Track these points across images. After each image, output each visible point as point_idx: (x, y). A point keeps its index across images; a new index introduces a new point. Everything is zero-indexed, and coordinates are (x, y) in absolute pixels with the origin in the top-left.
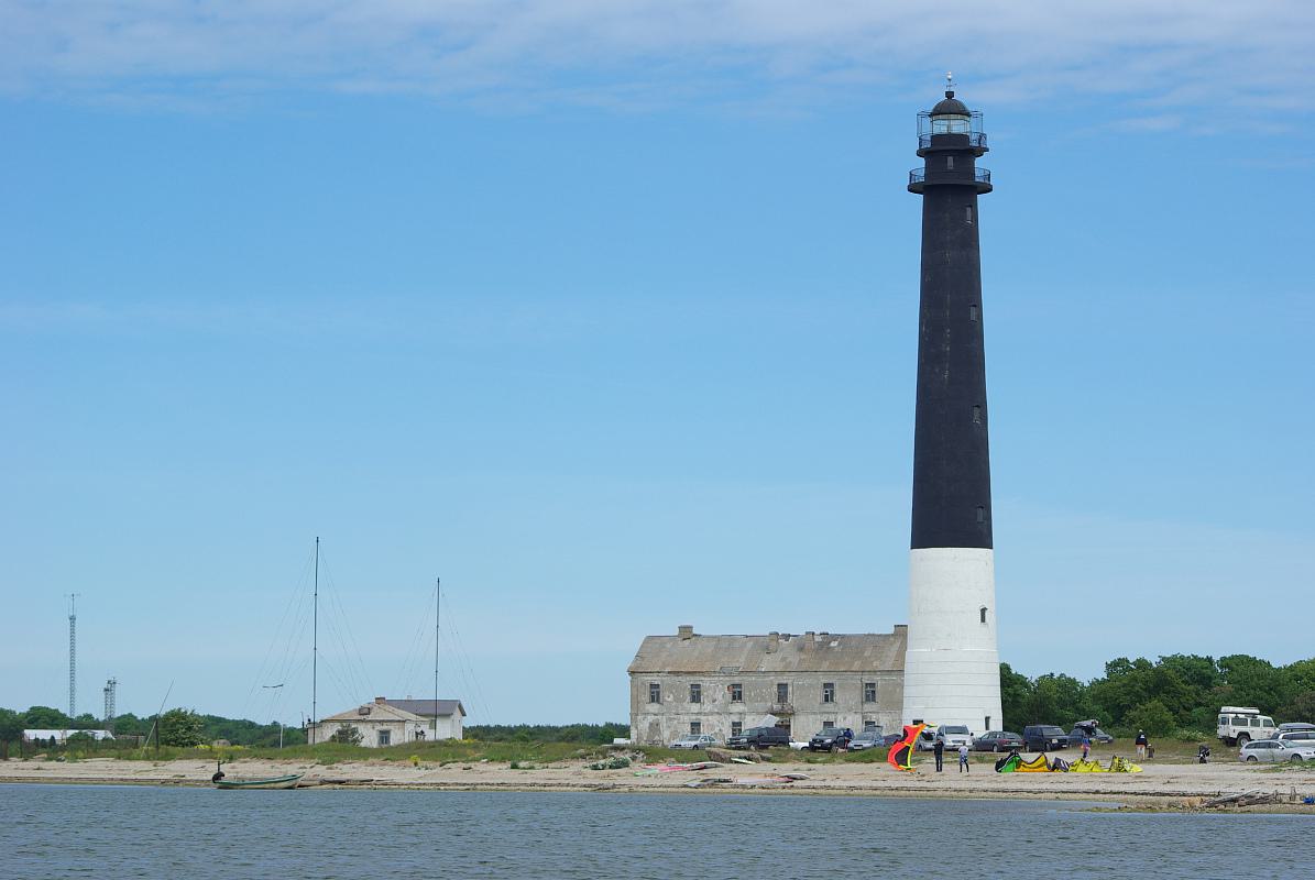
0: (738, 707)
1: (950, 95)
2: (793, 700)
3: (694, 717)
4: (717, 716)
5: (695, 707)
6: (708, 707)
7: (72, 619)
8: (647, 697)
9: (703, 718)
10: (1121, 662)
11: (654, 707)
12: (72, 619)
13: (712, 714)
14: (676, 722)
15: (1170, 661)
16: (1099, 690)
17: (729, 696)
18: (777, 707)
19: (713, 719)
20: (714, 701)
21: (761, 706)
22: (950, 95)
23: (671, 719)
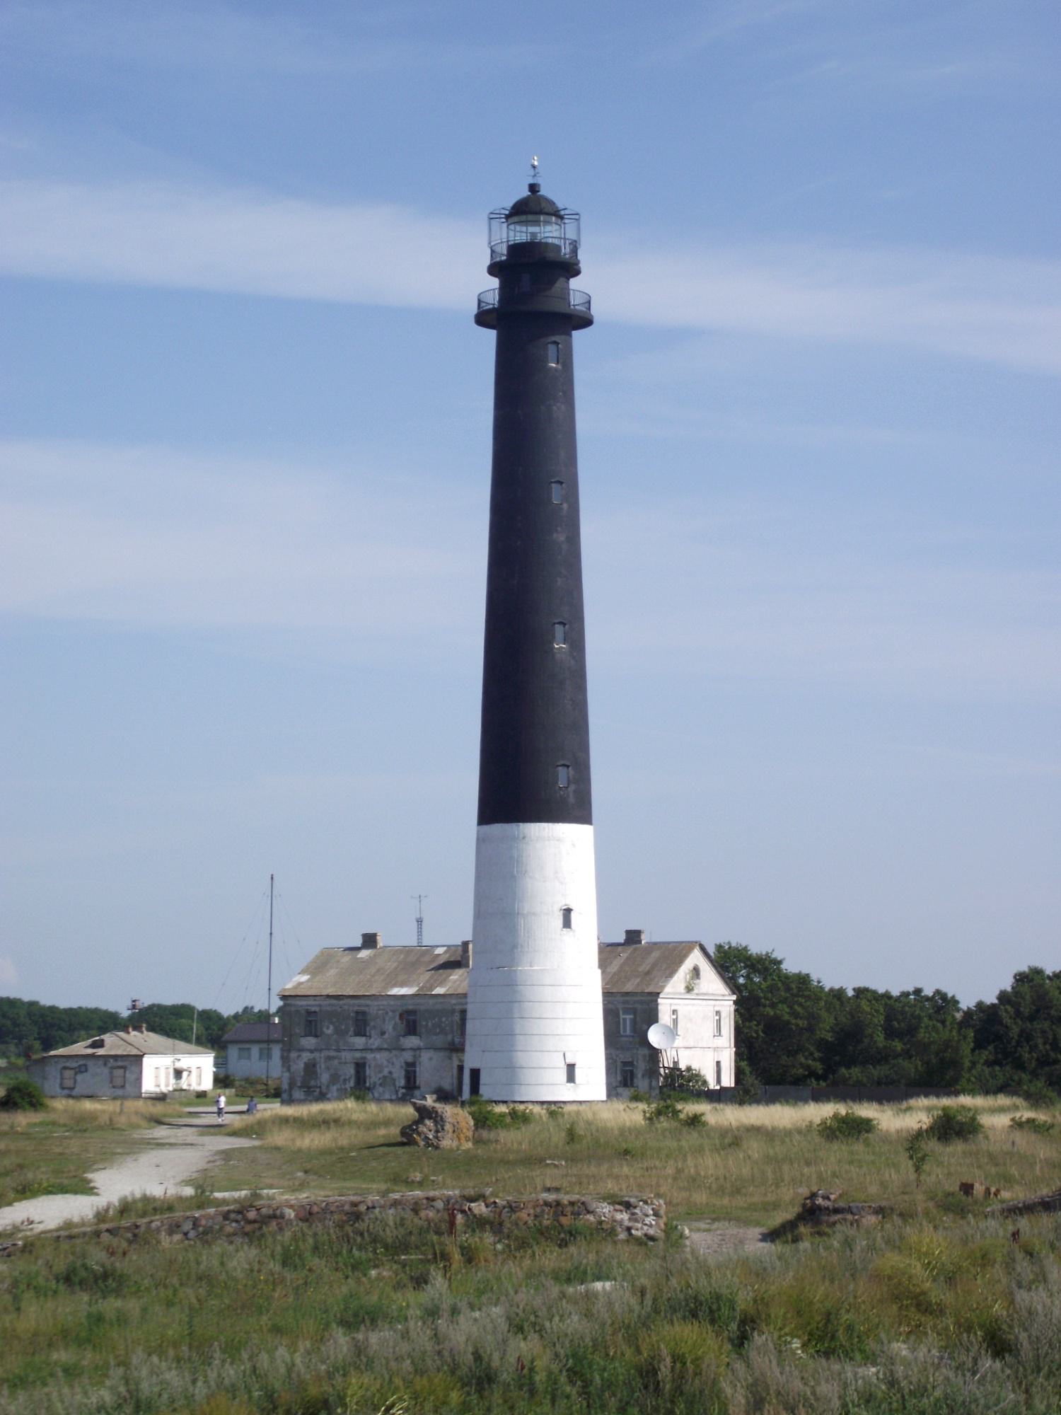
0: (413, 1041)
1: (533, 188)
3: (358, 1055)
4: (385, 1054)
5: (359, 1041)
7: (420, 921)
9: (369, 1056)
11: (309, 1042)
12: (420, 921)
13: (380, 1049)
14: (336, 1061)
15: (861, 992)
16: (986, 1022)
17: (402, 1027)
19: (381, 1057)
20: (383, 1033)
22: (533, 188)
23: (329, 1058)
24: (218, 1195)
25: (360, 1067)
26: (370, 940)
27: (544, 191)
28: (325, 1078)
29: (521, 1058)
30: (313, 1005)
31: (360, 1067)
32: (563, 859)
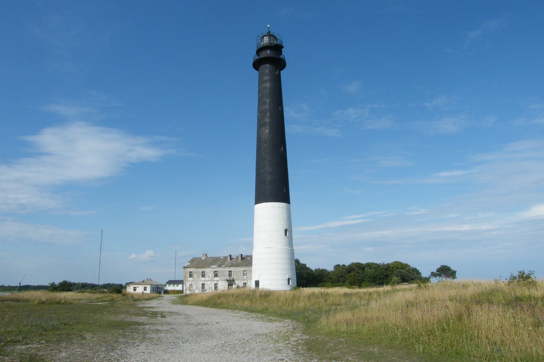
0: (216, 279)
2: (234, 276)
5: (203, 279)
6: (207, 279)
8: (188, 276)
10: (338, 266)
11: (191, 279)
12: (271, 59)
13: (208, 281)
17: (214, 275)
18: (228, 278)
21: (224, 278)
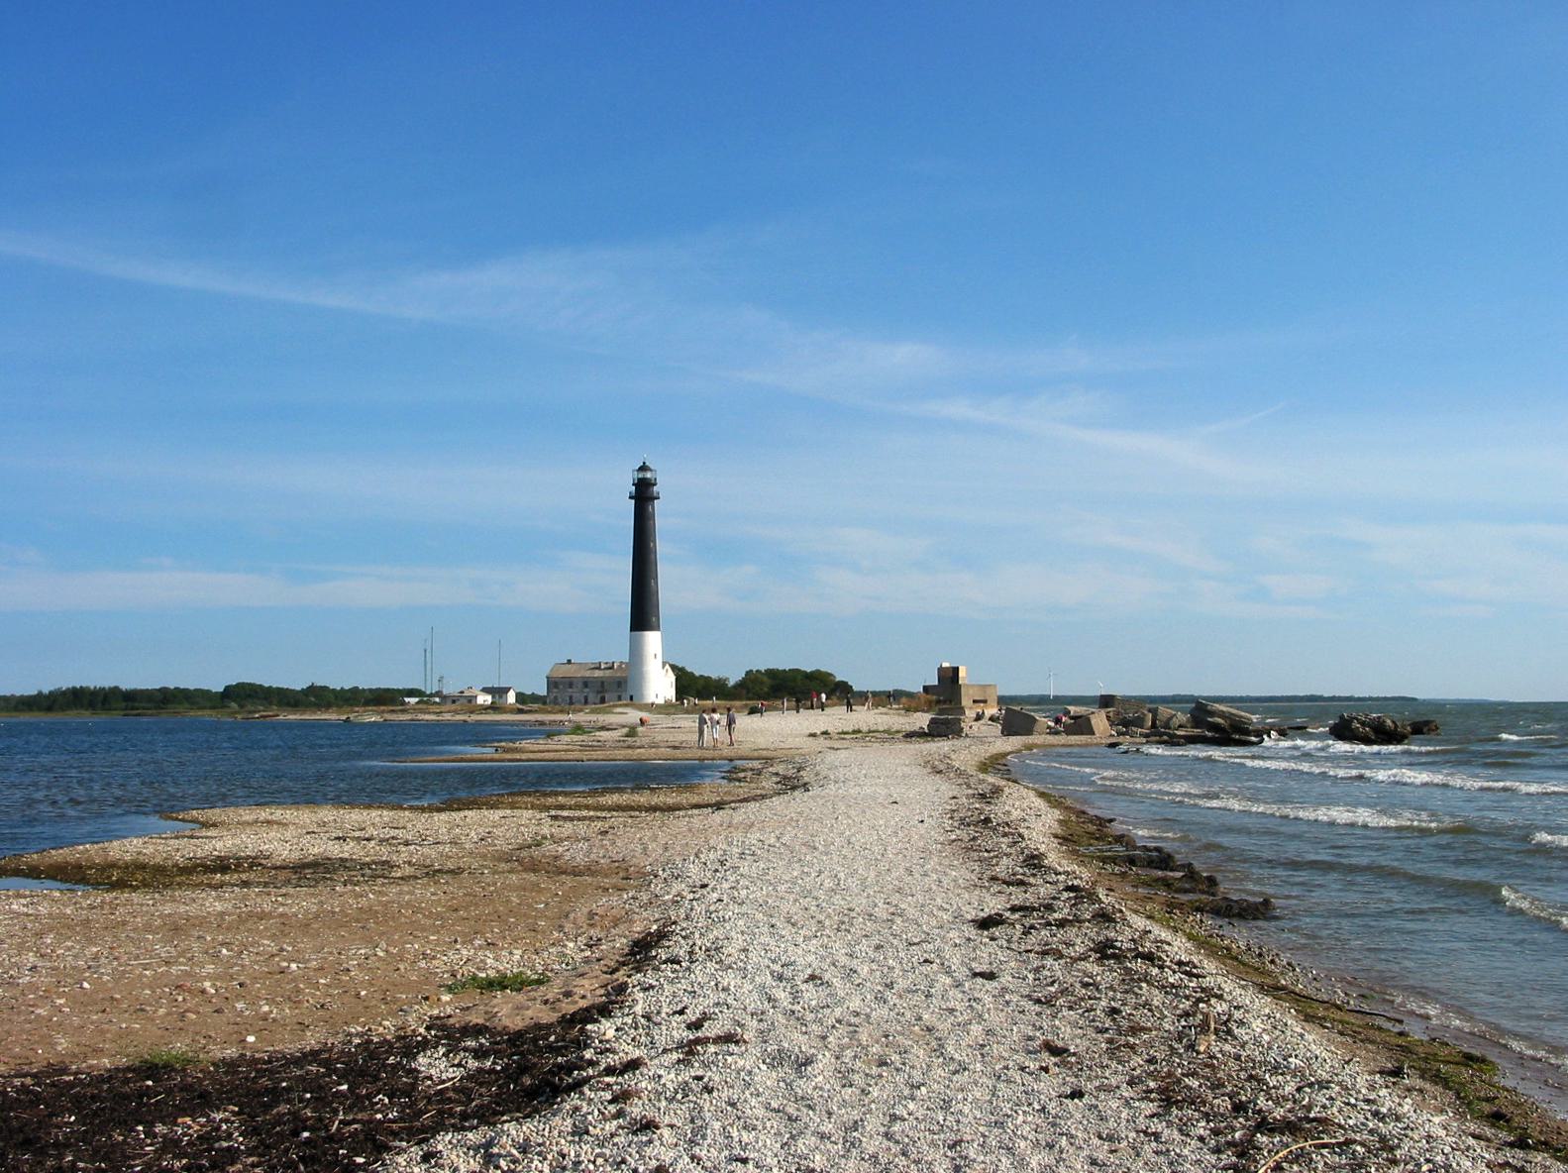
0: (586, 690)
1: (644, 463)
5: (570, 690)
11: (555, 690)
15: (176, 688)
22: (644, 463)
24: (1504, 736)
25: (571, 698)
26: (569, 662)
27: (647, 464)
28: (560, 700)
29: (645, 693)
30: (557, 680)
31: (571, 698)
32: (652, 640)
